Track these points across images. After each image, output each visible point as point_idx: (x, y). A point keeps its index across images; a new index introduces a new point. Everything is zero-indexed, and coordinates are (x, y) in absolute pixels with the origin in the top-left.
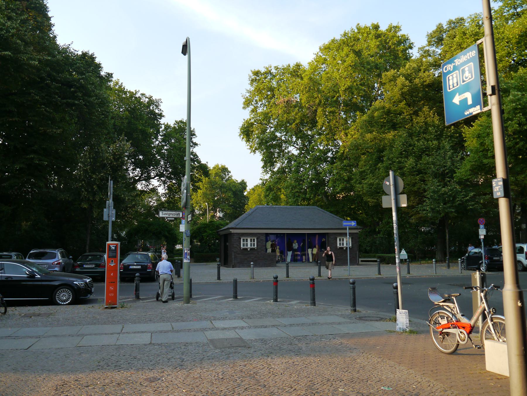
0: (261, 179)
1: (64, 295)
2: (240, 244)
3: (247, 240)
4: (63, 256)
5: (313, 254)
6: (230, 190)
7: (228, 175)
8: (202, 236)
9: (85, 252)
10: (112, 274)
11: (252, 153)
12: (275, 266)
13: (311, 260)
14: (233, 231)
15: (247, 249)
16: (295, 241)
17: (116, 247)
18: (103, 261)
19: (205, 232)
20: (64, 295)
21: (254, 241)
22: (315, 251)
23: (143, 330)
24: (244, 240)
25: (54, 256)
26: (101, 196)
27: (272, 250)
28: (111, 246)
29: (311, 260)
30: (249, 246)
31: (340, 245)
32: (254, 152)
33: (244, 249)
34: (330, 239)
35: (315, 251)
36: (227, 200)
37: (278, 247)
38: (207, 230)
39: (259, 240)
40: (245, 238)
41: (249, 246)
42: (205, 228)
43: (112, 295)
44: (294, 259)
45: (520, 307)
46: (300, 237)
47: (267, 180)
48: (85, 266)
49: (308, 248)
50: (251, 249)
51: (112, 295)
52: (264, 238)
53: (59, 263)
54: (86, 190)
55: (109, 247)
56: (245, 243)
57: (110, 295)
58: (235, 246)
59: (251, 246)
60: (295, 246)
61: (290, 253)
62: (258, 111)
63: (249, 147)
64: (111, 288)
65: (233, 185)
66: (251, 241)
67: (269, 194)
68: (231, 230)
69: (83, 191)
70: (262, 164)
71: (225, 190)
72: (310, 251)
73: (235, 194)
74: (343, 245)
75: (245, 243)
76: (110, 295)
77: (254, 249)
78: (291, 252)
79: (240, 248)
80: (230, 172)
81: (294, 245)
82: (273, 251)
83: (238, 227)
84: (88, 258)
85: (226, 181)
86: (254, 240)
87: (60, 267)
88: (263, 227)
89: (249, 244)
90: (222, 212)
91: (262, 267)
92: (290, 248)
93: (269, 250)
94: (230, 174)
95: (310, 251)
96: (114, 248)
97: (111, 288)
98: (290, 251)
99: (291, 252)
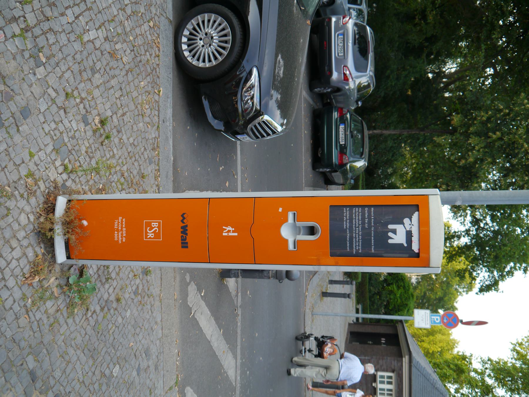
0: (471, 356)
1: (209, 41)
2: (383, 370)
3: (390, 383)
4: (360, 88)
6: (445, 294)
7: (464, 291)
8: (392, 284)
9: (369, 129)
10: (229, 231)
11: (512, 347)
14: (406, 360)
17: (405, 252)
18: (351, 159)
19: (399, 288)
20: (209, 41)
24: (390, 377)
25: (360, 68)
26: (477, 148)
28: (412, 223)
30: (380, 386)
32: (514, 350)
36: (432, 290)
38: (401, 290)
40: (393, 380)
42: (404, 287)
43: (120, 237)
47: (471, 363)
48: (342, 127)
51: (120, 237)
53: (346, 79)
54: (489, 119)
55: (401, 211)
57: (120, 223)
58: (381, 362)
59: (381, 389)
63: (520, 341)
64: (153, 230)
65: (450, 298)
66: (388, 390)
67: (451, 369)
68: (407, 357)
69: (487, 113)
70: (495, 358)
71: (444, 288)
73: (440, 299)
76: (120, 223)
80: (467, 294)
83: (413, 369)
84: (358, 131)
85: (456, 289)
87: (339, 81)
90: (417, 282)
94: (464, 294)
96: (398, 237)
97: (153, 230)
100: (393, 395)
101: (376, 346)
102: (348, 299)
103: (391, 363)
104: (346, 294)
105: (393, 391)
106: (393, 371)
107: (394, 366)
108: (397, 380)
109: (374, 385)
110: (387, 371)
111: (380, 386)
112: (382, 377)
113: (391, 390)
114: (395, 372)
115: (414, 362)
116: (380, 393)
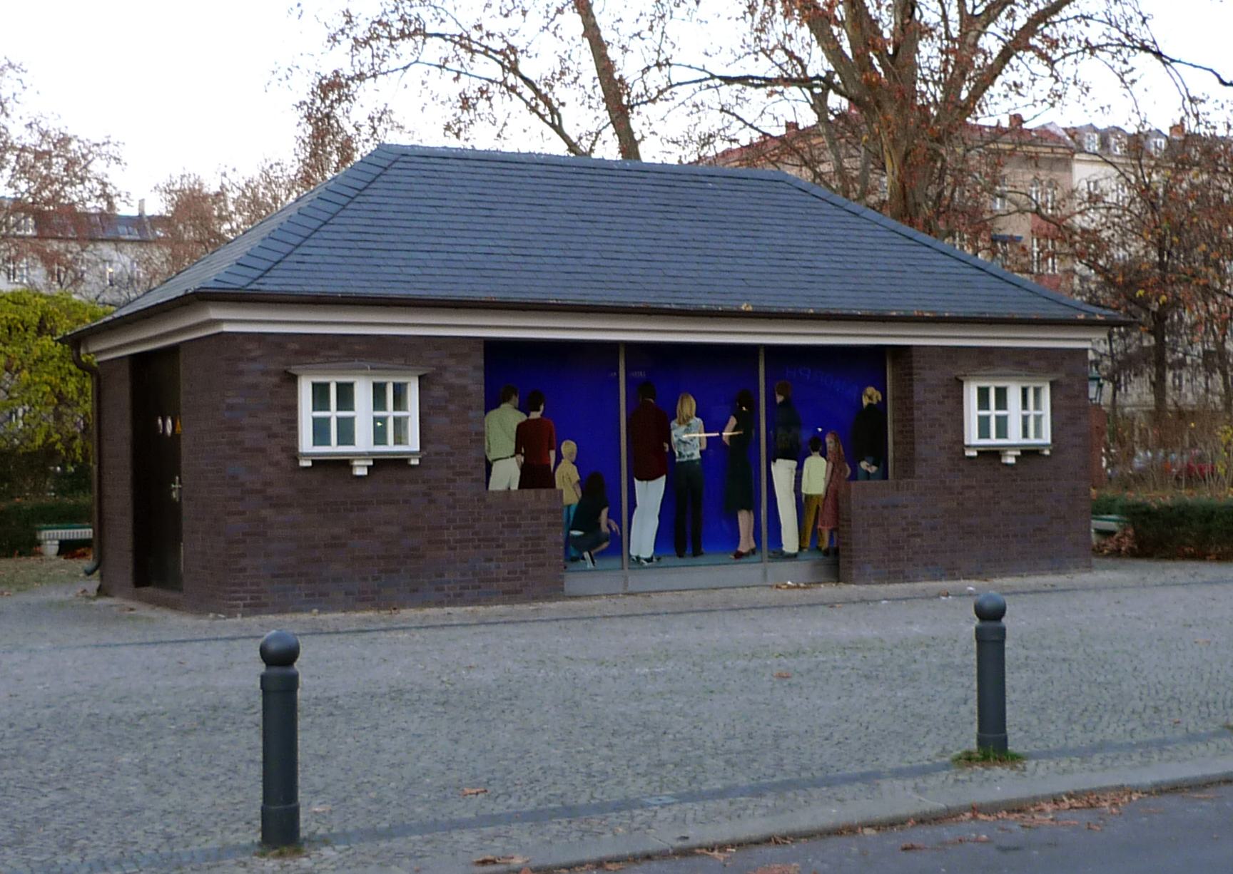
2: (292, 424)
3: (346, 393)
5: (802, 503)
12: (554, 591)
13: (790, 541)
15: (342, 465)
16: (688, 406)
21: (399, 402)
22: (817, 473)
23: (834, 840)
24: (320, 392)
27: (524, 469)
29: (790, 541)
30: (364, 441)
31: (984, 433)
33: (321, 464)
34: (920, 393)
35: (817, 473)
37: (569, 448)
39: (438, 392)
40: (992, 386)
41: (364, 441)
44: (686, 534)
45: (406, 460)
46: (716, 375)
49: (772, 458)
50: (381, 464)
52: (472, 379)
56: (333, 414)
59: (379, 436)
60: (690, 438)
61: (650, 494)
62: (1032, 177)
66: (379, 402)
68: (214, 313)
72: (782, 471)
74: (1002, 431)
75: (333, 414)
77: (399, 463)
78: (661, 483)
79: (294, 455)
81: (678, 433)
82: (536, 475)
83: (270, 285)
86: (400, 391)
88: (480, 294)
89: (368, 422)
91: (457, 599)
92: (654, 456)
93: (507, 473)
95: (782, 471)
98: (649, 476)
99: (661, 483)
100: (1038, 385)
101: (183, 463)
102: (1005, 621)
103: (255, 386)
104: (979, 633)
105: (1025, 385)
106: (293, 380)
107: (265, 373)
108: (328, 360)
109: (360, 471)
110: (292, 409)
111: (1015, 436)
112: (321, 430)
113: (379, 390)
114: (294, 369)
115: (239, 282)
116: (398, 441)
